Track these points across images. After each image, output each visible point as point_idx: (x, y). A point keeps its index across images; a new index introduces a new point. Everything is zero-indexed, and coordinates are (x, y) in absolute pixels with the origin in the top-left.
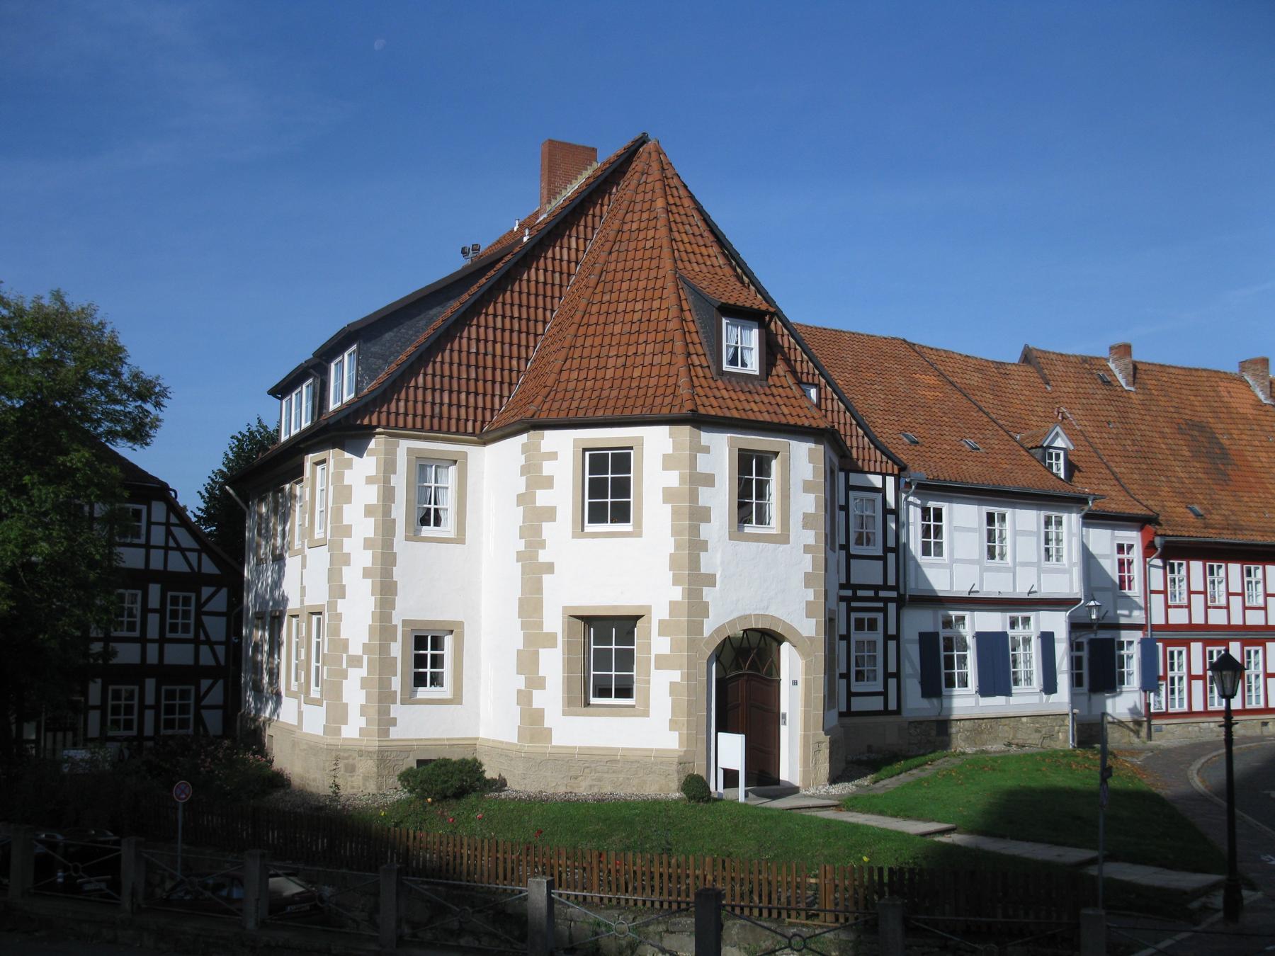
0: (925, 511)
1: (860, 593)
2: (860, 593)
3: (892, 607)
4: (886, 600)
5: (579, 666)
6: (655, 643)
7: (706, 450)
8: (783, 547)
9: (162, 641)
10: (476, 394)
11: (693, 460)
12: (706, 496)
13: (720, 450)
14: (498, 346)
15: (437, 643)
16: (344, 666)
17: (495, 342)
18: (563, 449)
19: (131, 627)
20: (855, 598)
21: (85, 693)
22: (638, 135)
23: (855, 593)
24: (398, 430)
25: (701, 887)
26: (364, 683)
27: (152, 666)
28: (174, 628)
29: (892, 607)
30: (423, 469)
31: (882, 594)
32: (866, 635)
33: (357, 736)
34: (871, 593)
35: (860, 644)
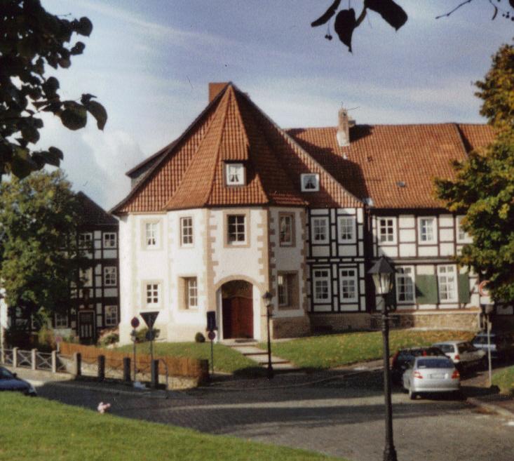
0: (383, 223)
1: (344, 260)
2: (344, 260)
3: (335, 267)
4: (358, 263)
5: (183, 295)
6: (201, 287)
7: (213, 216)
8: (247, 249)
9: (103, 288)
10: (165, 196)
11: (208, 220)
12: (213, 233)
13: (219, 217)
14: (173, 177)
15: (156, 287)
17: (171, 175)
18: (174, 217)
19: (113, 282)
20: (341, 262)
21: (95, 308)
23: (341, 260)
24: (136, 212)
27: (99, 298)
28: (108, 282)
29: (335, 267)
30: (148, 225)
31: (356, 260)
32: (348, 278)
34: (350, 260)
35: (318, 283)
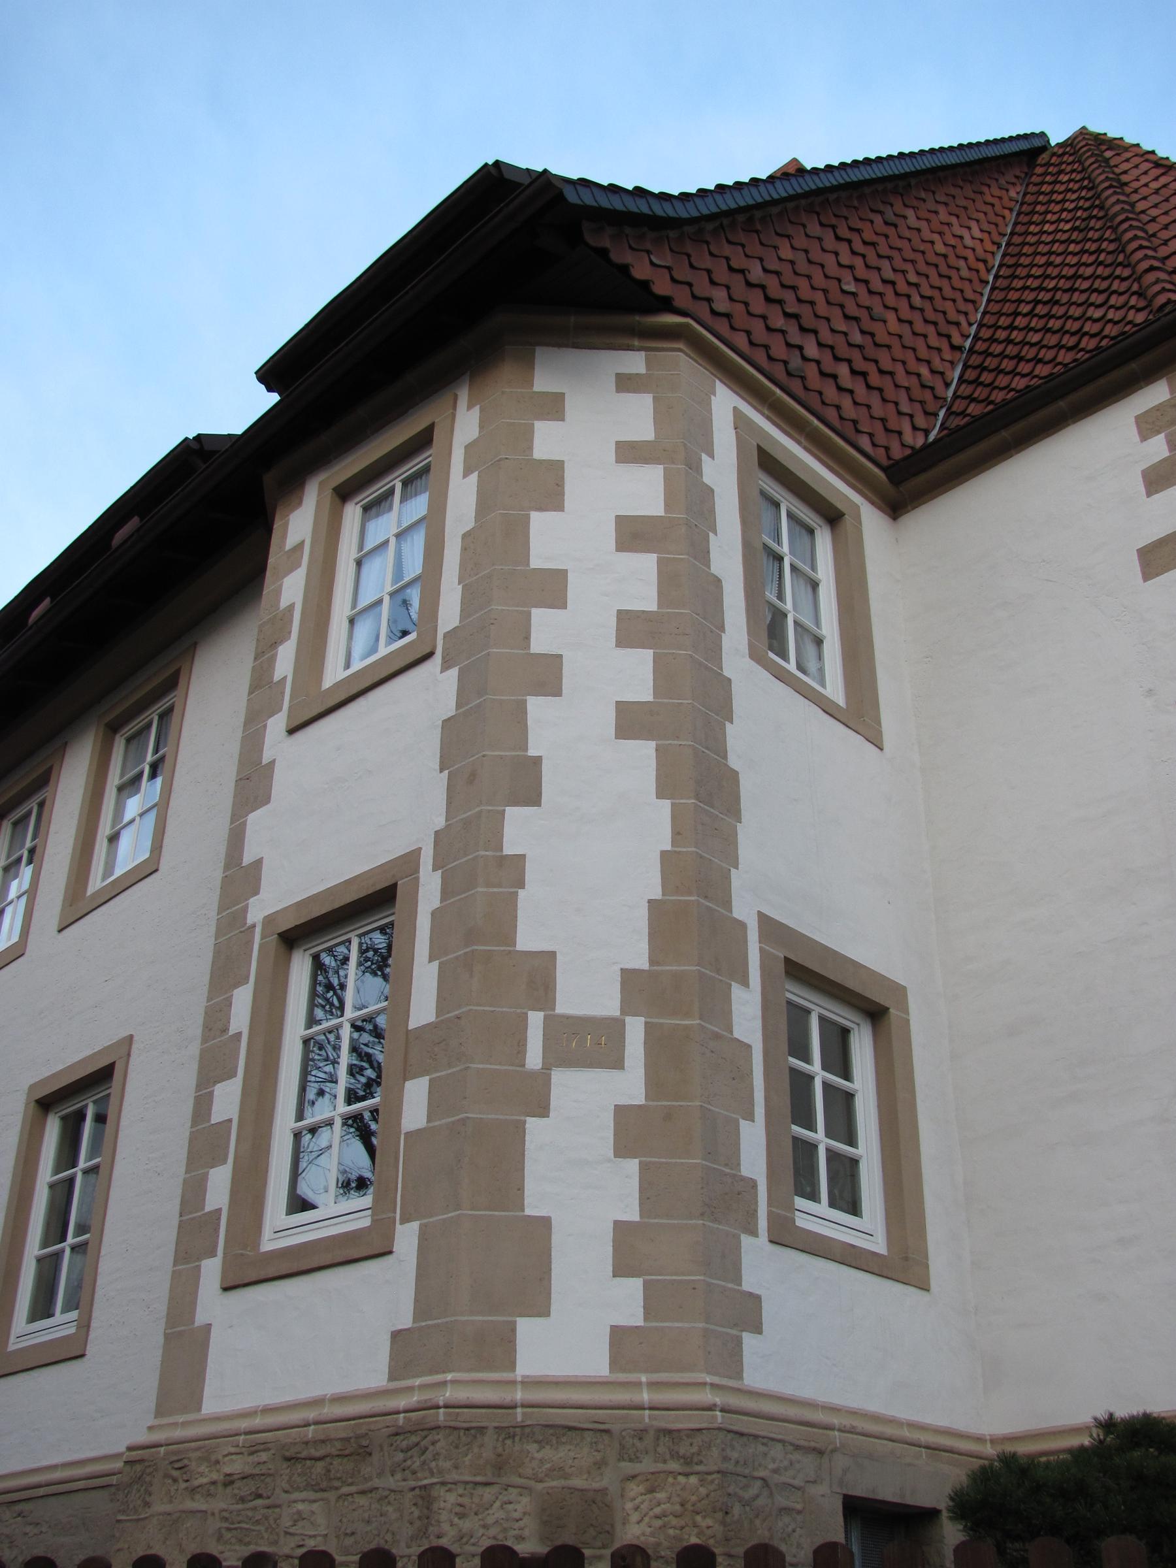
16: (534, 1058)
22: (300, 736)
25: (587, 1552)
26: (632, 1131)
33: (598, 1364)
